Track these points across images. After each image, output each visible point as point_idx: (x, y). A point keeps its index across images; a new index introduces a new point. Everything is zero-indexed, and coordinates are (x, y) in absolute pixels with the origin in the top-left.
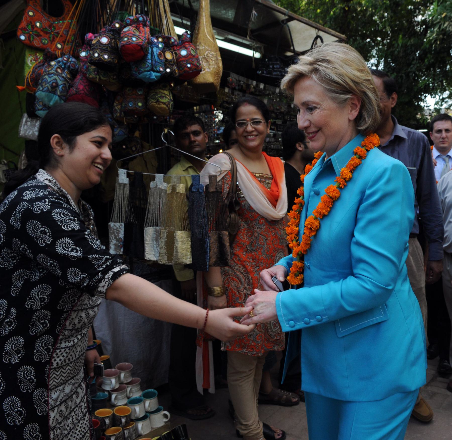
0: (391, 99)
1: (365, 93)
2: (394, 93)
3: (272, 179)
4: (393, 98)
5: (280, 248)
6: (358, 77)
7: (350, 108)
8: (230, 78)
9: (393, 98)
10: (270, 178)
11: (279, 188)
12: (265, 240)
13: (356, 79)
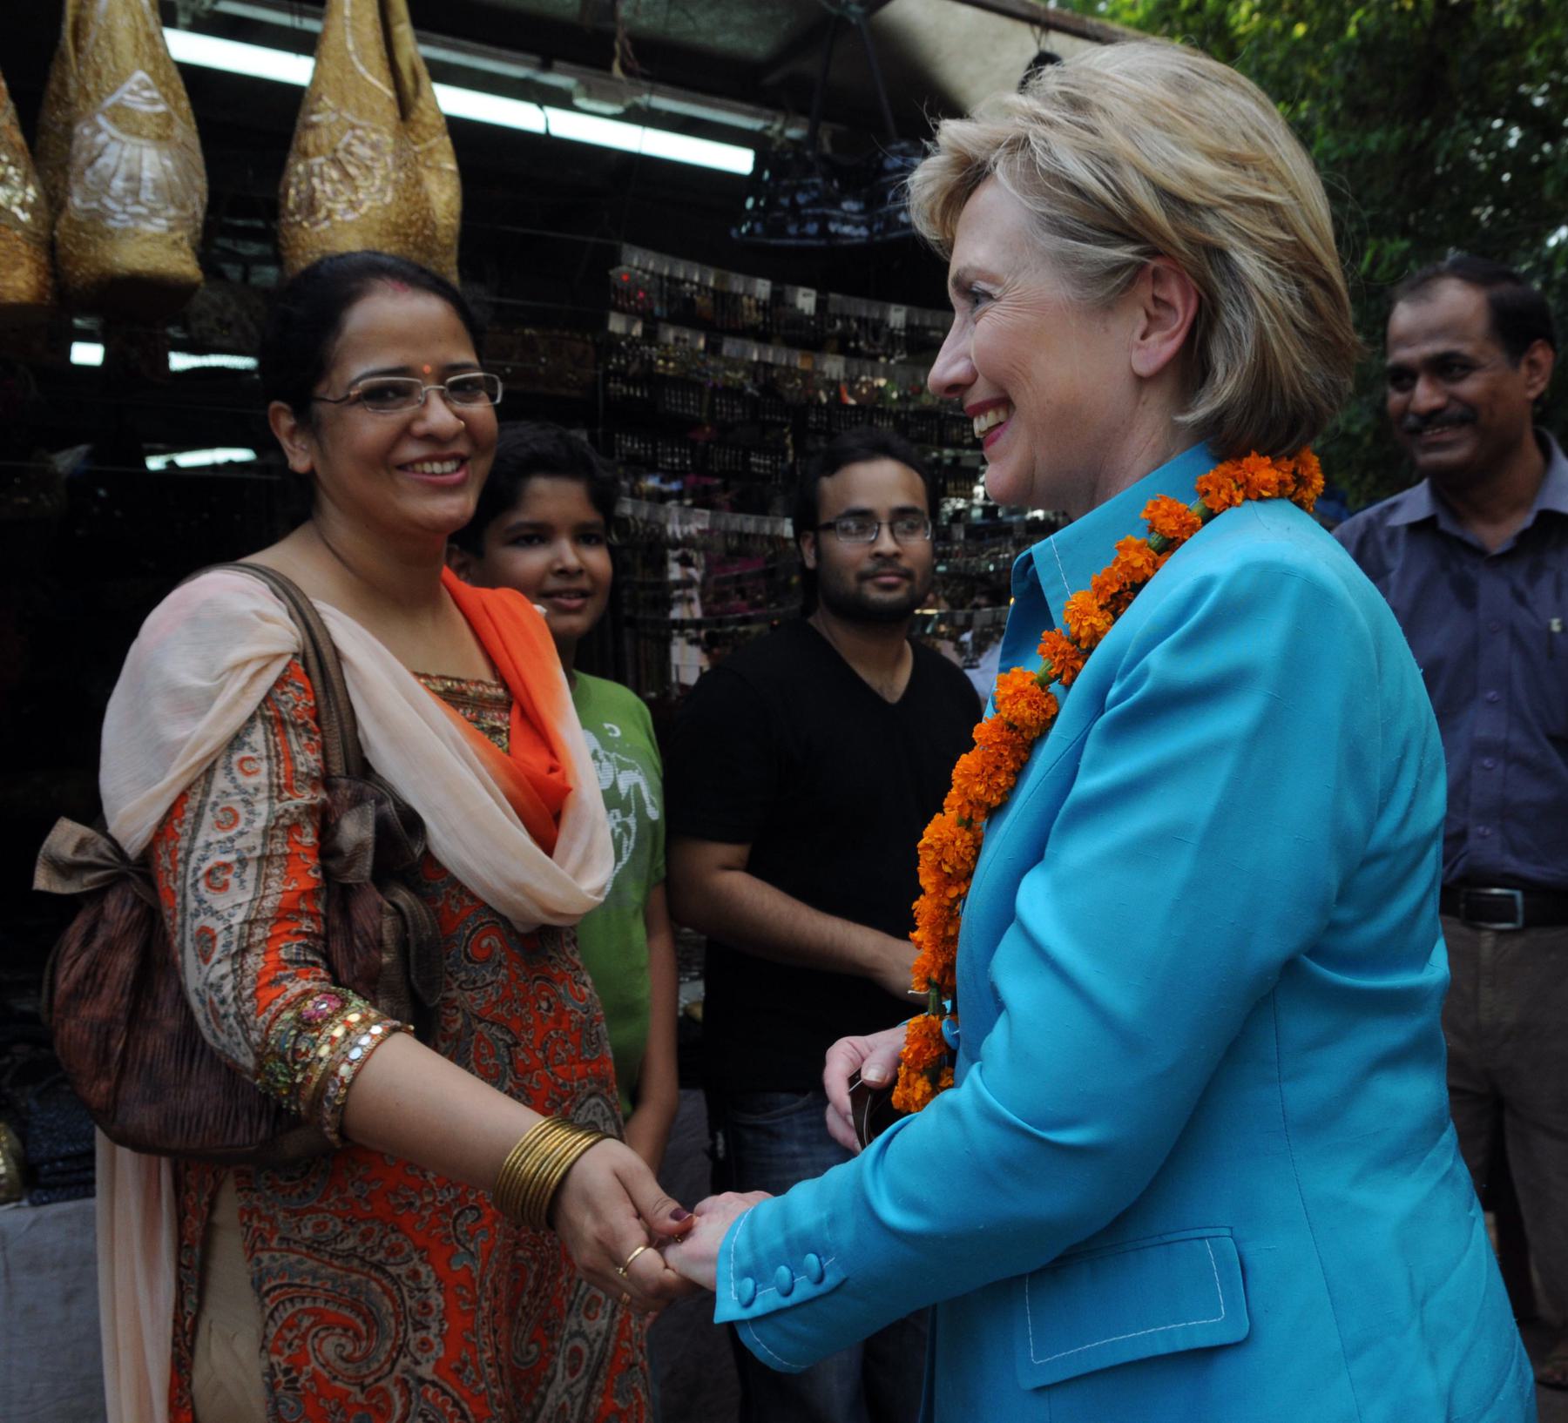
0: (1524, 369)
1: (1218, 254)
2: (1539, 342)
3: (508, 709)
4: (1533, 364)
5: (586, 1075)
6: (1192, 179)
7: (1143, 322)
8: (624, 268)
9: (1533, 364)
10: (497, 700)
11: (558, 749)
12: (504, 1051)
13: (1179, 186)
